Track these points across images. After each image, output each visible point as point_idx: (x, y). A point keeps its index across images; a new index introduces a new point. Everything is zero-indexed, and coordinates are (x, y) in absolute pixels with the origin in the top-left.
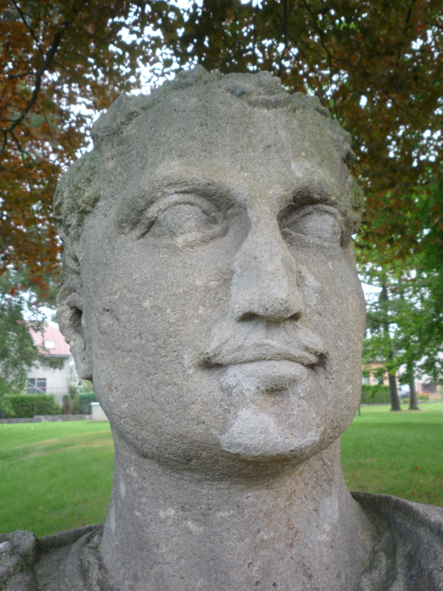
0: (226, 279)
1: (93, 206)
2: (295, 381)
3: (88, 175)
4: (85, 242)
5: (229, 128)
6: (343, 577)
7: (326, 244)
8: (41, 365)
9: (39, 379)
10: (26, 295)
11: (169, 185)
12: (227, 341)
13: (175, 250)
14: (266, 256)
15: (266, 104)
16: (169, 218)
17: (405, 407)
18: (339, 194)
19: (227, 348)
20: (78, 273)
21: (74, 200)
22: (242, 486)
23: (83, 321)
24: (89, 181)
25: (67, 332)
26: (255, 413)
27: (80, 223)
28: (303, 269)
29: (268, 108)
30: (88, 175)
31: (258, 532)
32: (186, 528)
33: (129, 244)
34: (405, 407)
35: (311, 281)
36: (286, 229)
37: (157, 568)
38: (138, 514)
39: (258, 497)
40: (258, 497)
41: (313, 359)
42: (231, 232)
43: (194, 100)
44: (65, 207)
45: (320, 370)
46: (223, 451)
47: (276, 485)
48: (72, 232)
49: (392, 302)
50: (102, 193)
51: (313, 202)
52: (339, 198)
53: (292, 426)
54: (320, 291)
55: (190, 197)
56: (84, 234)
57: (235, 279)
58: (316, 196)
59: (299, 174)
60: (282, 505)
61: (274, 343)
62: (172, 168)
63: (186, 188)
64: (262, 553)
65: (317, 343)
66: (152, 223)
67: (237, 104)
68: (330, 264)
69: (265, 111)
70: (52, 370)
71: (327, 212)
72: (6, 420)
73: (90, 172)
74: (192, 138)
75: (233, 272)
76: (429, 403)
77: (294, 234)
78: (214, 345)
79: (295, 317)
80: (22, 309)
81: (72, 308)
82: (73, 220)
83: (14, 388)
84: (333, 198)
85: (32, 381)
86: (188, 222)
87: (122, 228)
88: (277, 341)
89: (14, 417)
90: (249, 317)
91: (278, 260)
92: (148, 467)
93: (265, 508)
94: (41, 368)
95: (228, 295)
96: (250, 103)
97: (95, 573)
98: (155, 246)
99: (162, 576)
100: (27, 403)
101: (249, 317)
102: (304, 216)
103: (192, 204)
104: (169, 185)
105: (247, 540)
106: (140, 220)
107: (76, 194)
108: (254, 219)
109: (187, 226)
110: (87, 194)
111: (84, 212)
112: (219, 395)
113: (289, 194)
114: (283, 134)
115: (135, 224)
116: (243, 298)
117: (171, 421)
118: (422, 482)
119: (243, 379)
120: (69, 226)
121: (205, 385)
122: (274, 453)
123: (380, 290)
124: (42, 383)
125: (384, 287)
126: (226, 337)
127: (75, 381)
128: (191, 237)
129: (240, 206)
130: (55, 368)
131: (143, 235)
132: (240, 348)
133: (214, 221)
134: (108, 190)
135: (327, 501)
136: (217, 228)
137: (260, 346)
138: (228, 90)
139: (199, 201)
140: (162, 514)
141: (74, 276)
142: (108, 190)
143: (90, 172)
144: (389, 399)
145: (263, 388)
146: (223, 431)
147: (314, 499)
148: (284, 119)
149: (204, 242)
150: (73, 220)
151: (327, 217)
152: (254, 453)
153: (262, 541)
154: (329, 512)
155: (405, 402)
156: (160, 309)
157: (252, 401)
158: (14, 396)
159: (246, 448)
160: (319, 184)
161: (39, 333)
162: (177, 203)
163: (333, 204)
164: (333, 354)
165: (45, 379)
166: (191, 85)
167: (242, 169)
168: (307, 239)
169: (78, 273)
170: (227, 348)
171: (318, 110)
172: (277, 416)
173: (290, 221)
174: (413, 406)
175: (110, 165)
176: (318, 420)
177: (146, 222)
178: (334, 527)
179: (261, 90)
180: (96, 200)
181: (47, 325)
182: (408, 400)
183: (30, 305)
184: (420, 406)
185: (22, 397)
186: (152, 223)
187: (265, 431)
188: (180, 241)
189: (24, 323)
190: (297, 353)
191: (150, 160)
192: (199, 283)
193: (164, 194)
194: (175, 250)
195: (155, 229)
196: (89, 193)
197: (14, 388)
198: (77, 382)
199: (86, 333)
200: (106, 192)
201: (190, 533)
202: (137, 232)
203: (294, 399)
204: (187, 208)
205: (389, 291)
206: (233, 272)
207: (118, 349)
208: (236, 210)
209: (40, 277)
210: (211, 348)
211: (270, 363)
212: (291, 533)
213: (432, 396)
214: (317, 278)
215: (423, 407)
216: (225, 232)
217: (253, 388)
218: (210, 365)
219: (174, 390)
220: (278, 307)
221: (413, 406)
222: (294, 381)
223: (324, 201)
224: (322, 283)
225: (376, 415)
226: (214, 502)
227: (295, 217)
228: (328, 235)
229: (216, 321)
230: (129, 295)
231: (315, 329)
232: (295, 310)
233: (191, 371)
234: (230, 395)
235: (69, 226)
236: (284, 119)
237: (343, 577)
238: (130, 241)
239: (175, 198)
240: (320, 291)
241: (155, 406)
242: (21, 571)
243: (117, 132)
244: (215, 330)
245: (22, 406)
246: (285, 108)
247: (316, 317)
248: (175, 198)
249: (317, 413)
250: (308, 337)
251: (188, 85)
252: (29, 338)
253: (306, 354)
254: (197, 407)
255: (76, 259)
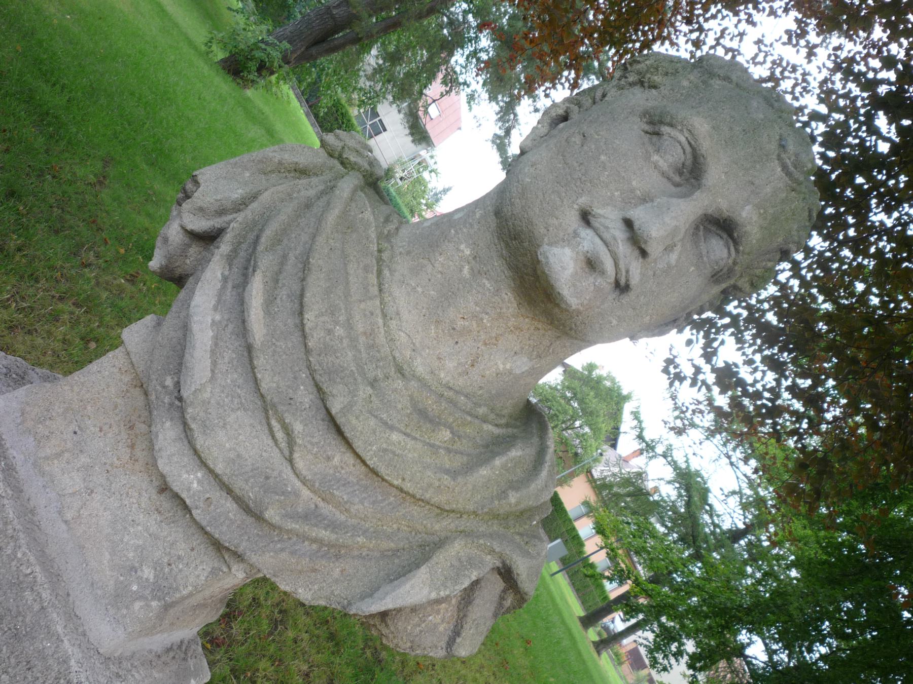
0: (645, 199)
1: (650, 87)
2: (603, 273)
3: (670, 71)
4: (621, 95)
5: (751, 150)
6: (481, 392)
7: (705, 259)
8: (405, 114)
9: (380, 121)
10: (485, 42)
11: (690, 131)
12: (607, 218)
13: (647, 158)
14: (673, 214)
15: (784, 167)
16: (667, 143)
17: (592, 634)
18: (747, 250)
19: (602, 220)
20: (594, 103)
21: (647, 71)
22: (513, 285)
23: (562, 125)
24: (667, 74)
25: (546, 117)
26: (571, 258)
27: (632, 84)
28: (678, 248)
29: (783, 170)
30: (670, 71)
31: (487, 314)
32: (463, 267)
33: (636, 127)
34: (592, 634)
35: (673, 257)
36: (702, 227)
37: (425, 262)
38: (453, 231)
39: (509, 301)
40: (509, 301)
41: (623, 282)
42: (679, 189)
43: (761, 116)
44: (639, 66)
45: (617, 293)
46: (536, 252)
47: (523, 310)
48: (623, 82)
49: (733, 550)
50: (662, 88)
51: (731, 236)
52: (743, 252)
53: (574, 285)
54: (669, 266)
55: (688, 149)
56: (626, 92)
57: (649, 205)
58: (735, 235)
59: (744, 214)
60: (510, 324)
61: (621, 248)
62: (701, 126)
63: (693, 143)
64: (474, 323)
65: (635, 280)
66: (658, 134)
67: (773, 146)
68: (693, 268)
69: (779, 169)
70: (407, 131)
71: (729, 249)
72: (306, 108)
73: (673, 71)
74: (731, 129)
75: (652, 201)
76: (616, 669)
77: (701, 233)
78: (600, 211)
79: (644, 253)
80: (462, 48)
81: (566, 112)
82: (632, 78)
83: (355, 96)
84: (741, 248)
85: (375, 114)
86: (672, 155)
87: (645, 116)
88: (624, 249)
89: (316, 116)
90: (628, 223)
91: (674, 223)
92: (489, 220)
93: (504, 310)
94: (402, 116)
95: (636, 206)
96: (779, 155)
97: (391, 227)
98: (644, 144)
99: (422, 267)
100: (343, 123)
101: (628, 223)
102: (717, 234)
103: (684, 153)
104: (690, 131)
105: (478, 309)
106: (655, 125)
107: (652, 70)
108: (694, 197)
109: (668, 156)
110: (656, 78)
111: (641, 83)
112: (570, 230)
113: (726, 214)
114: (768, 189)
115: (651, 123)
116: (638, 214)
117: (537, 211)
118: (515, 652)
119: (588, 240)
120: (626, 77)
121: (572, 219)
122: (552, 282)
123: (741, 526)
124: (379, 129)
125: (749, 529)
126: (609, 217)
127: (403, 171)
128: (661, 163)
129: (699, 185)
130: (412, 134)
131: (647, 132)
132: (607, 228)
133: (681, 174)
134: (666, 92)
135: (525, 360)
136: (677, 179)
137: (615, 239)
138: (781, 136)
139: (689, 156)
140: (462, 247)
141: (590, 101)
142: (666, 92)
143: (673, 71)
144: (594, 608)
145: (589, 255)
146: (550, 244)
147: (523, 348)
148: (781, 185)
149: (663, 174)
150: (632, 78)
151: (726, 251)
152: (546, 270)
153: (482, 319)
154: (518, 363)
155: (599, 634)
156: (604, 168)
157: (577, 253)
158: (343, 102)
159: (547, 263)
160: (745, 232)
161: (443, 89)
162: (679, 142)
163: (737, 251)
164: (632, 295)
165: (385, 130)
166: (773, 108)
167: (726, 173)
168: (702, 244)
169: (594, 103)
170: (602, 220)
171: (810, 212)
172: (576, 273)
173: (709, 226)
174: (602, 645)
175: (685, 83)
176: (586, 302)
177: (657, 129)
178: (510, 372)
179: (793, 158)
180: (655, 87)
181: (458, 93)
182: (605, 635)
183: (474, 54)
184: (604, 655)
185: (347, 112)
186: (658, 134)
187: (563, 268)
188: (655, 158)
189: (447, 61)
190: (622, 266)
191: (701, 109)
192: (634, 183)
193: (681, 131)
194: (647, 158)
195: (655, 138)
196: (657, 79)
197: (355, 96)
198: (403, 175)
199: (555, 132)
200: (664, 91)
201: (461, 271)
202: (647, 128)
203: (591, 279)
204: (680, 151)
205: (746, 540)
206: (652, 201)
207: (563, 156)
208: (696, 184)
209: (523, 50)
210: (598, 210)
211: (607, 251)
212: (494, 341)
213: (626, 667)
214: (677, 261)
215: (605, 661)
216: (677, 185)
217: (586, 248)
218: (586, 217)
219: (559, 203)
220: (645, 235)
221: (602, 645)
222: (603, 273)
223: (736, 243)
224: (676, 266)
225: (563, 598)
226: (492, 273)
227: (714, 229)
228: (712, 257)
229: (615, 206)
230: (602, 144)
231: (643, 275)
232: (649, 249)
233: (576, 206)
234: (574, 237)
235: (626, 77)
236: (781, 185)
237: (481, 392)
238: (638, 126)
239: (683, 139)
240: (669, 266)
241: (541, 197)
242: (364, 176)
243: (712, 75)
244: (609, 208)
245: (337, 119)
246: (790, 182)
247: (651, 273)
248: (683, 139)
249: (590, 300)
250: (635, 269)
251: (772, 106)
252: (431, 77)
253: (624, 274)
254: (555, 222)
255: (604, 96)
